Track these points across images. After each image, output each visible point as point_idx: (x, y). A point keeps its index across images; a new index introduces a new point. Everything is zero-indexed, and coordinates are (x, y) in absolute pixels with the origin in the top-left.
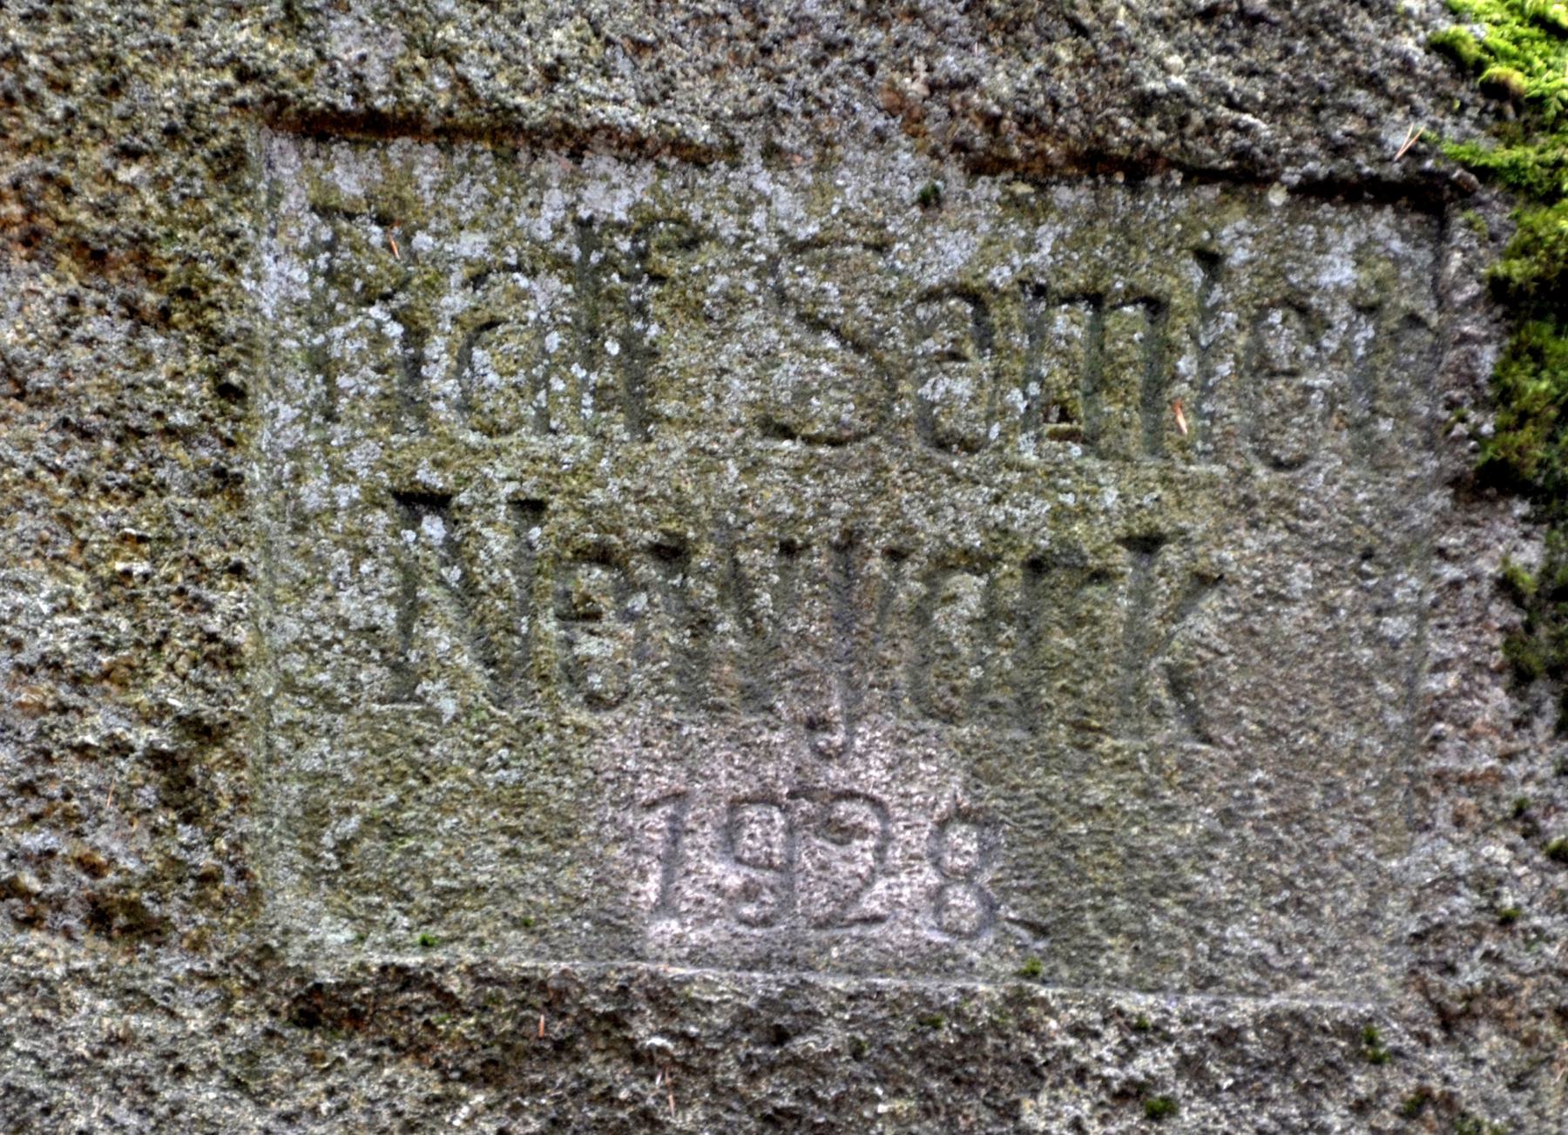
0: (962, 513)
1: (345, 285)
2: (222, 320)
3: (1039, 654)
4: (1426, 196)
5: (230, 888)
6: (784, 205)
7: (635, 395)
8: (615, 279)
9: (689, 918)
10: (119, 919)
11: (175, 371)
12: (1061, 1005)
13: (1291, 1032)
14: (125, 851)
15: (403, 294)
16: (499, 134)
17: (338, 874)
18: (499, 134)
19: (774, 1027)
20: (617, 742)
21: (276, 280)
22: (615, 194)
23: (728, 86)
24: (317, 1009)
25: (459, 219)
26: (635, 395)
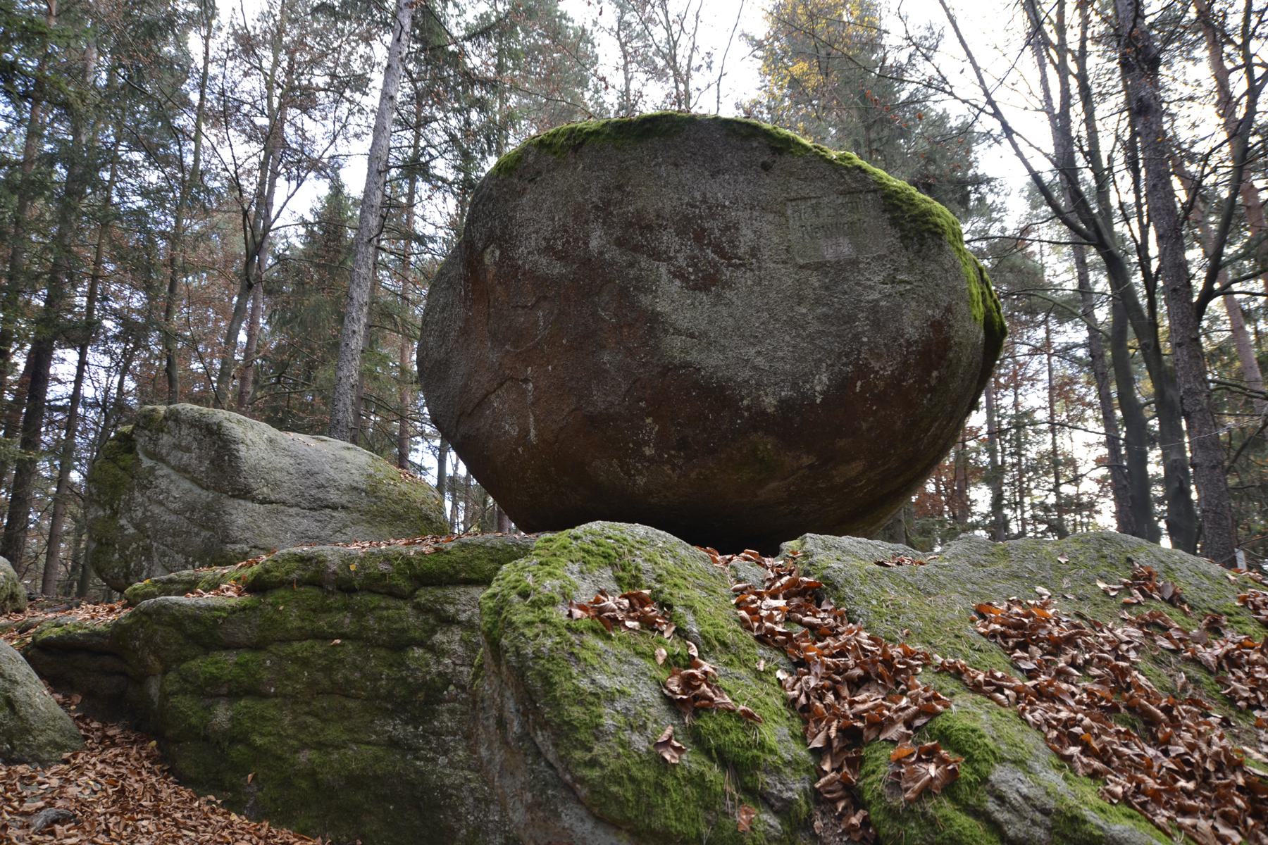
0: (845, 220)
1: (795, 211)
2: (939, 167)
3: (853, 231)
4: (875, 191)
5: (793, 259)
6: (826, 200)
7: (818, 216)
8: (814, 208)
9: (829, 254)
10: (784, 262)
11: (783, 220)
12: (861, 257)
13: (879, 256)
14: (784, 257)
15: (799, 211)
16: (804, 199)
17: (801, 256)
18: (804, 199)
19: (838, 262)
20: (821, 242)
21: (789, 212)
22: (814, 201)
23: (346, 678)
24: (801, 267)
25: (802, 206)
26: (818, 216)
